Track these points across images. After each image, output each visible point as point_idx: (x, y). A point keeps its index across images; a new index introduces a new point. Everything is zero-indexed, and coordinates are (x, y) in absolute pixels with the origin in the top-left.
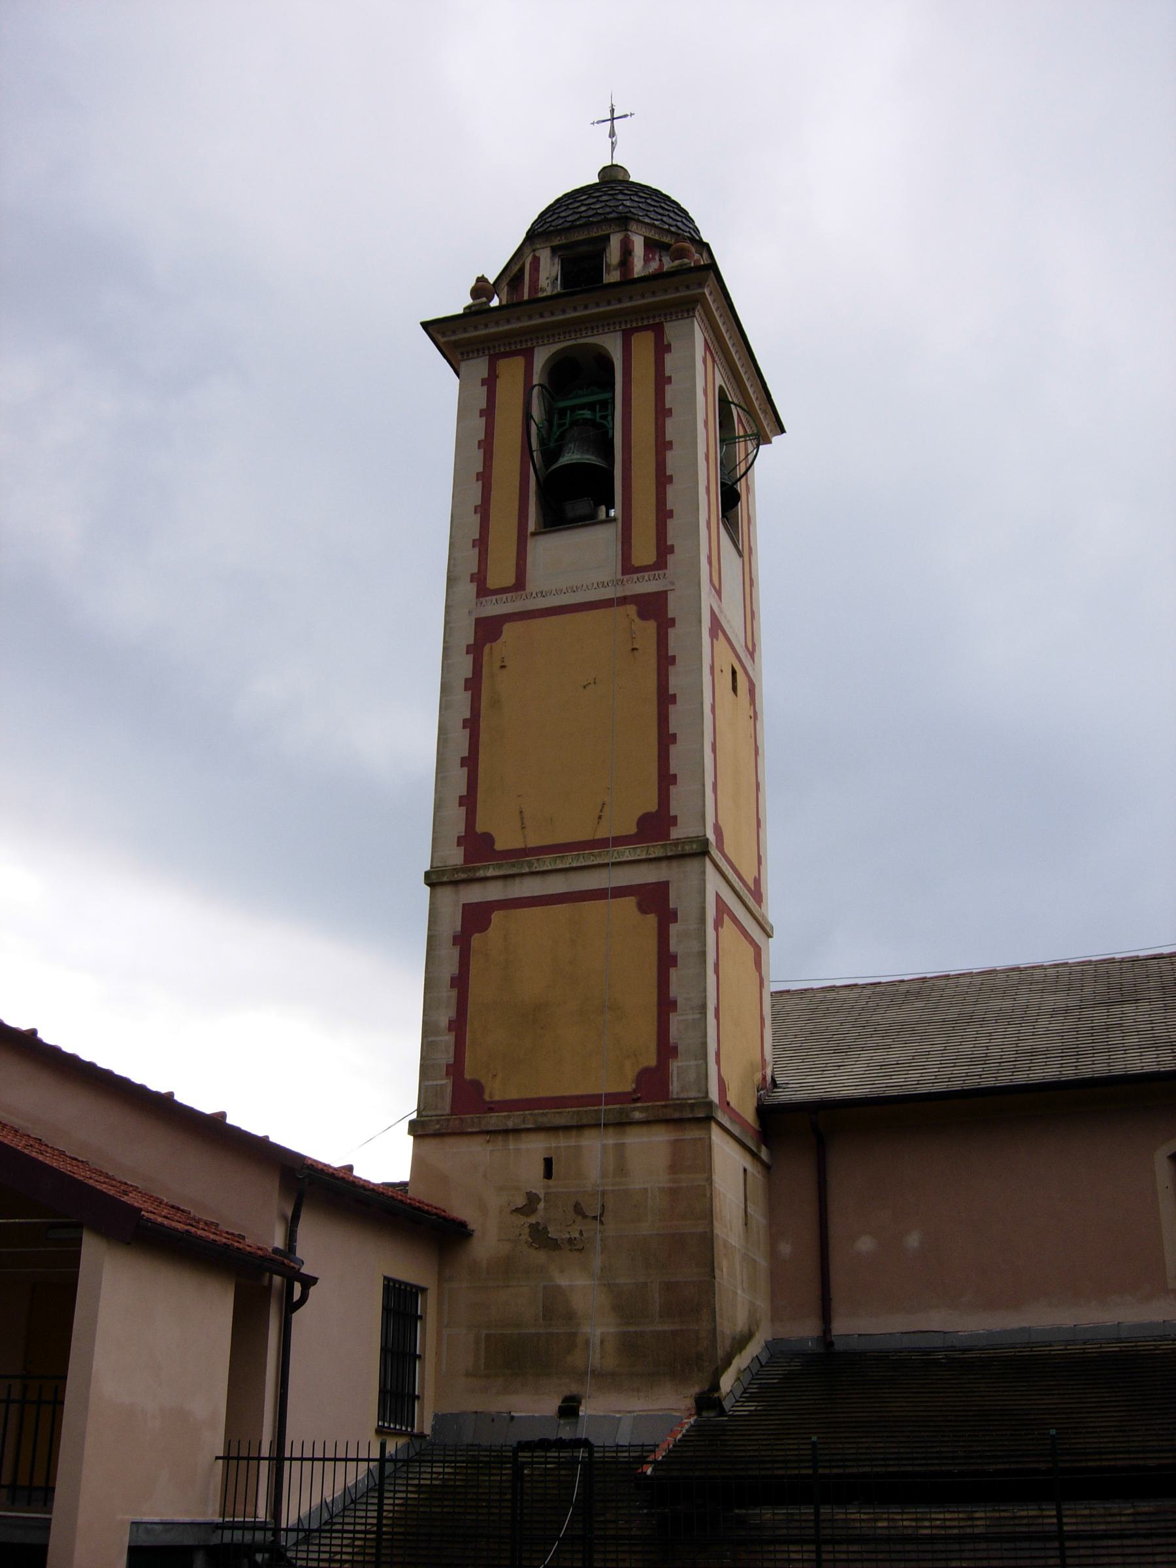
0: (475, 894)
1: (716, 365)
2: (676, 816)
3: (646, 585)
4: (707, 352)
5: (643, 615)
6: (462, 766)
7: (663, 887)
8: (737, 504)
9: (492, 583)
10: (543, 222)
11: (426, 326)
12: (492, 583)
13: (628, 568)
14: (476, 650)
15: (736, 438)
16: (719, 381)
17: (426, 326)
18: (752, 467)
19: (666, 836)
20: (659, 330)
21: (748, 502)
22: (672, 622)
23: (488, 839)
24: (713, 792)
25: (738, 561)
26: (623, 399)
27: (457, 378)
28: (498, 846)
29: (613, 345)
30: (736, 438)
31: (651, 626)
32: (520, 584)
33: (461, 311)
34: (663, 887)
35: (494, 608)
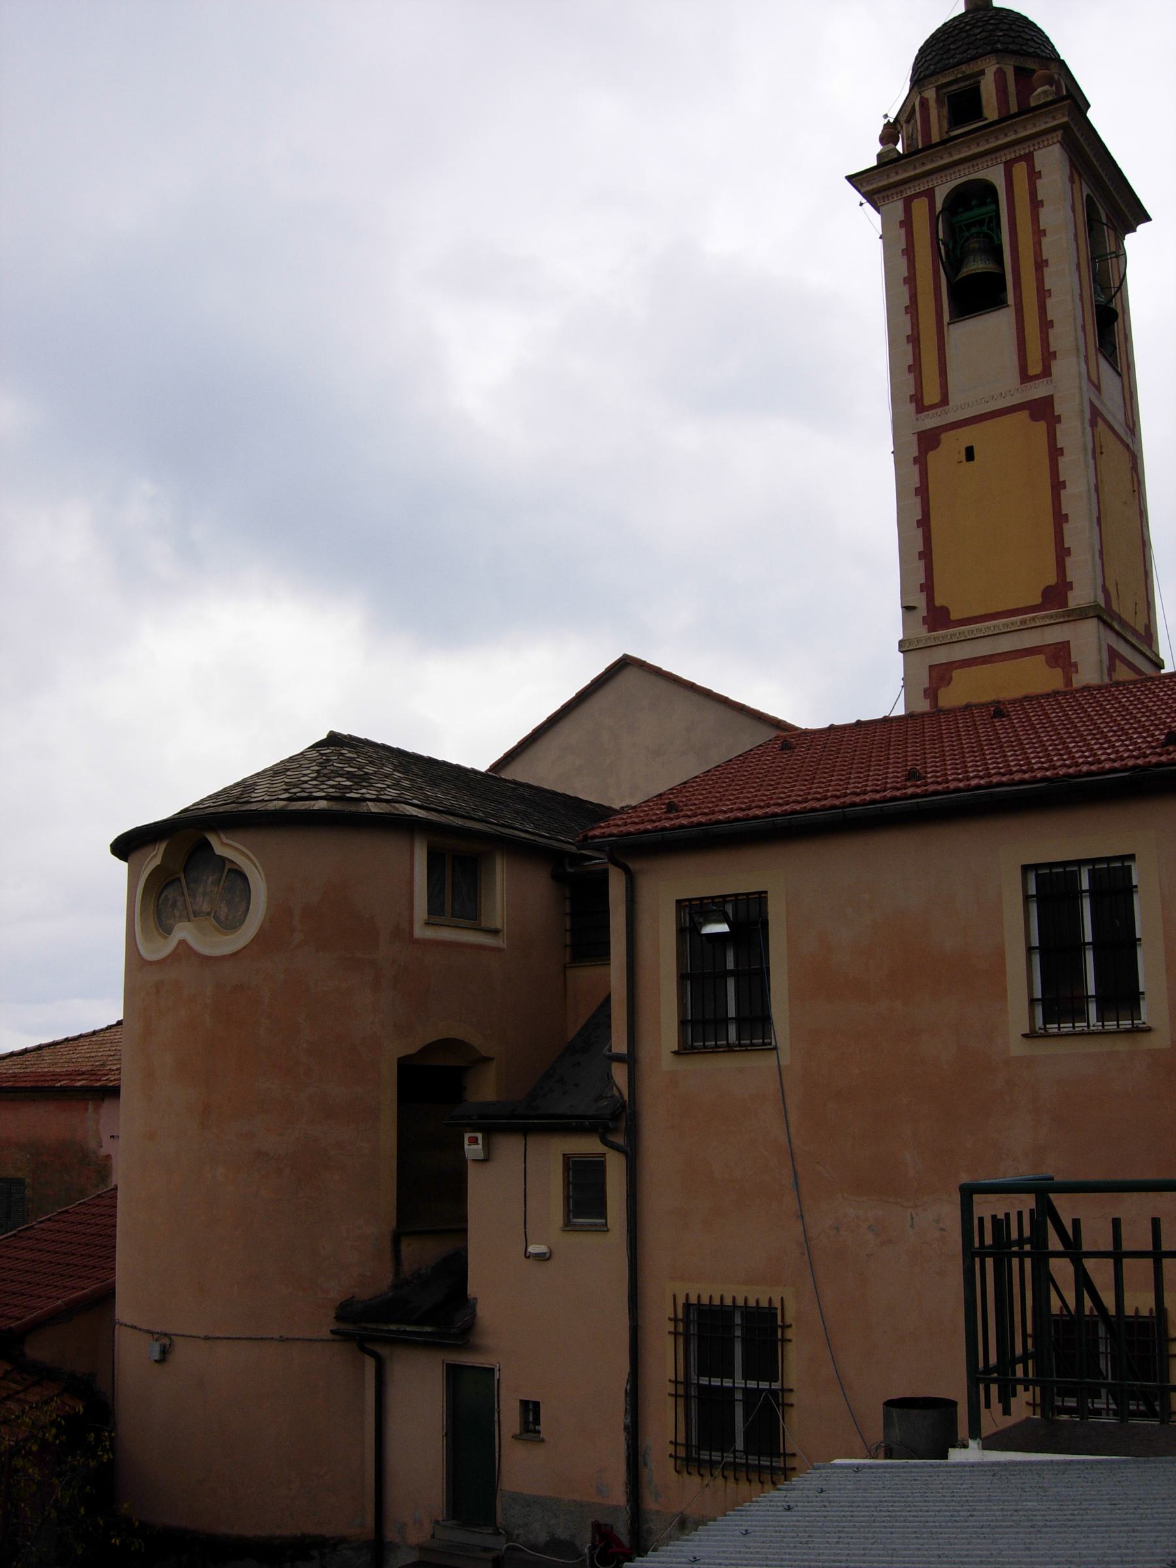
0: (942, 656)
1: (1083, 181)
2: (1072, 582)
3: (1038, 391)
4: (1074, 172)
5: (1034, 417)
6: (914, 464)
7: (1065, 646)
8: (1114, 324)
9: (927, 402)
10: (924, 60)
11: (850, 178)
12: (927, 402)
13: (1025, 377)
14: (921, 461)
15: (1107, 254)
16: (1086, 191)
17: (850, 178)
18: (1145, 1034)
19: (1066, 604)
20: (1029, 158)
21: (1124, 399)
22: (1058, 419)
23: (945, 611)
24: (1098, 525)
25: (1117, 379)
26: (1010, 228)
27: (876, 213)
28: (953, 617)
29: (995, 175)
30: (1107, 254)
31: (1042, 426)
32: (944, 401)
33: (873, 162)
34: (1065, 646)
35: (931, 421)
